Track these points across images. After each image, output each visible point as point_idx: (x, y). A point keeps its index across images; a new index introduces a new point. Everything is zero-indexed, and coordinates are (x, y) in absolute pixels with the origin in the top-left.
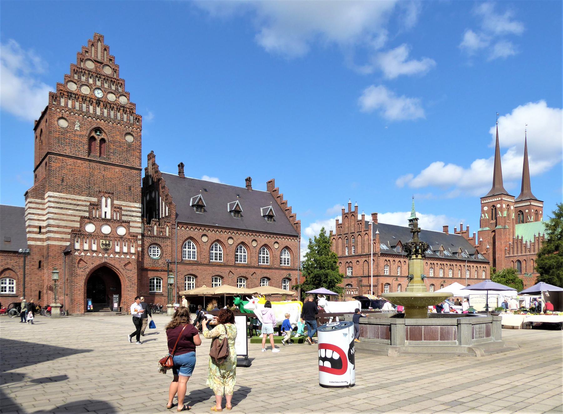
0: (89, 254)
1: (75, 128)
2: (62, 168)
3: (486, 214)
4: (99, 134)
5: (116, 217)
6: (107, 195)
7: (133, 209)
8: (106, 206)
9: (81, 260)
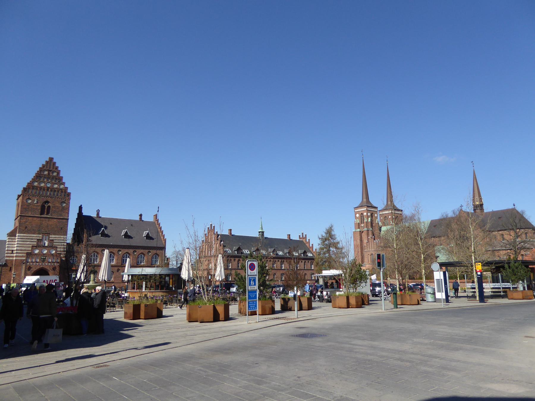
2: (26, 222)
3: (358, 220)
7: (33, 238)
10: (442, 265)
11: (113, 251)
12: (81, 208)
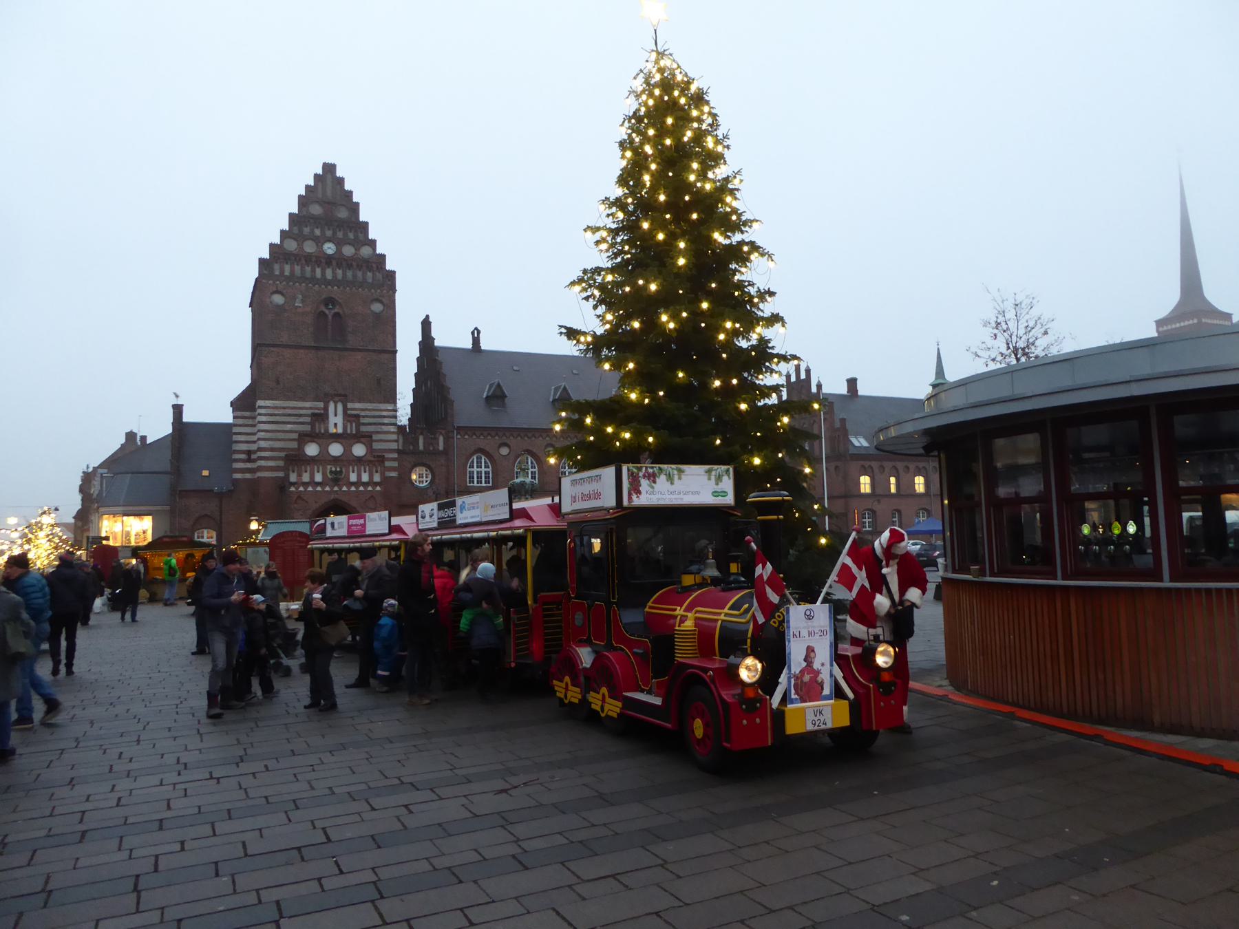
0: (310, 489)
1: (296, 305)
4: (331, 307)
6: (336, 399)
7: (385, 413)
8: (336, 415)
9: (299, 497)
11: (531, 449)
12: (426, 324)
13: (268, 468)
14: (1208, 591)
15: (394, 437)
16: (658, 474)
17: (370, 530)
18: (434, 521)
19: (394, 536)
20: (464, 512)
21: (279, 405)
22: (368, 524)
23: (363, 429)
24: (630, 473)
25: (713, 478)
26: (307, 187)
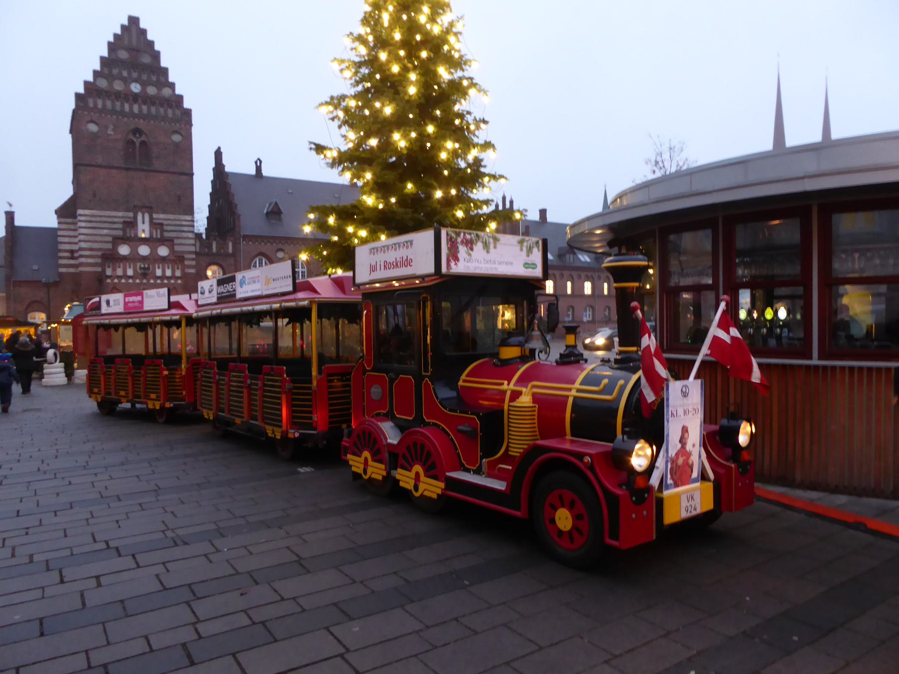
1: (109, 132)
5: (157, 235)
6: (144, 210)
8: (143, 223)
10: (281, 427)
12: (218, 154)
13: (88, 264)
14: (851, 369)
15: (192, 242)
16: (475, 242)
17: (147, 306)
18: (213, 297)
19: (173, 311)
20: (244, 286)
21: (96, 214)
22: (145, 300)
23: (166, 234)
24: (449, 238)
25: (524, 249)
26: (116, 36)
